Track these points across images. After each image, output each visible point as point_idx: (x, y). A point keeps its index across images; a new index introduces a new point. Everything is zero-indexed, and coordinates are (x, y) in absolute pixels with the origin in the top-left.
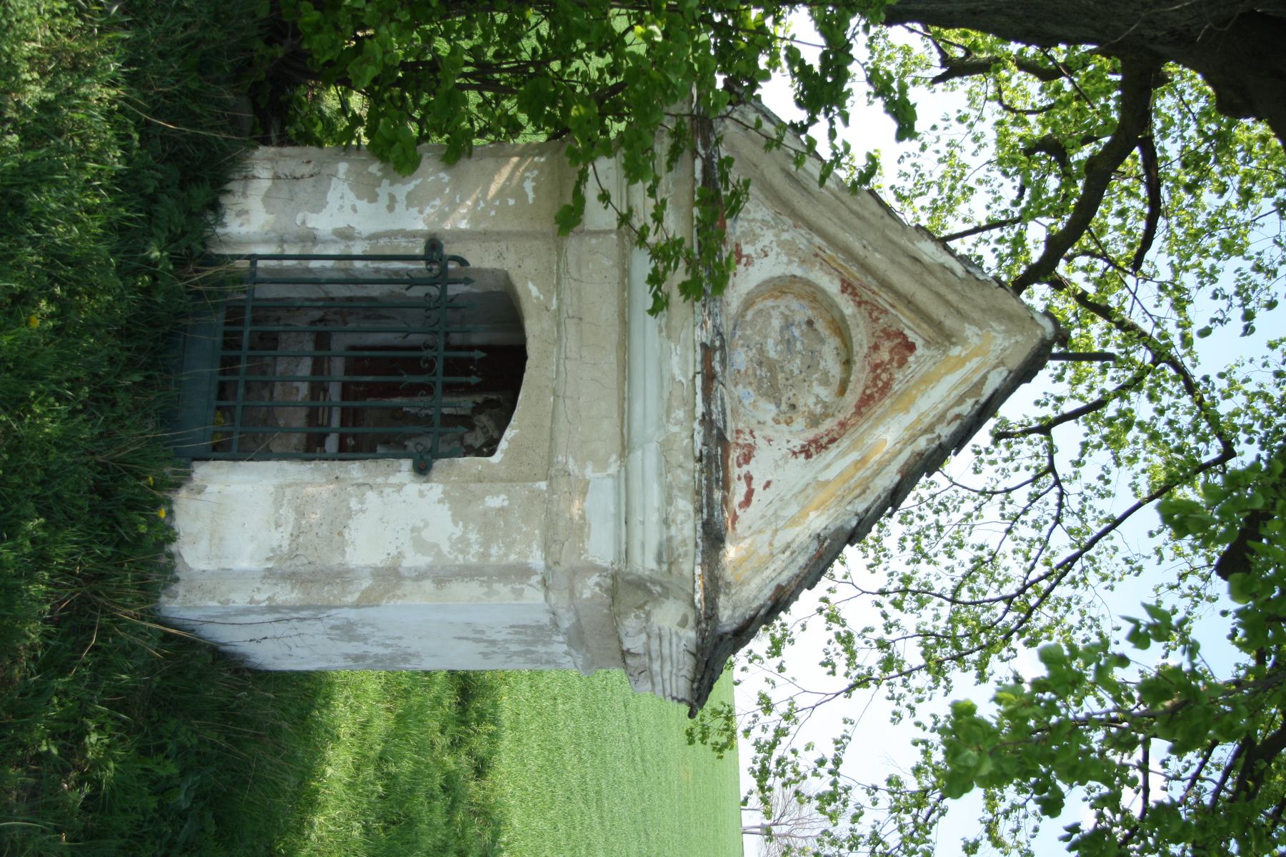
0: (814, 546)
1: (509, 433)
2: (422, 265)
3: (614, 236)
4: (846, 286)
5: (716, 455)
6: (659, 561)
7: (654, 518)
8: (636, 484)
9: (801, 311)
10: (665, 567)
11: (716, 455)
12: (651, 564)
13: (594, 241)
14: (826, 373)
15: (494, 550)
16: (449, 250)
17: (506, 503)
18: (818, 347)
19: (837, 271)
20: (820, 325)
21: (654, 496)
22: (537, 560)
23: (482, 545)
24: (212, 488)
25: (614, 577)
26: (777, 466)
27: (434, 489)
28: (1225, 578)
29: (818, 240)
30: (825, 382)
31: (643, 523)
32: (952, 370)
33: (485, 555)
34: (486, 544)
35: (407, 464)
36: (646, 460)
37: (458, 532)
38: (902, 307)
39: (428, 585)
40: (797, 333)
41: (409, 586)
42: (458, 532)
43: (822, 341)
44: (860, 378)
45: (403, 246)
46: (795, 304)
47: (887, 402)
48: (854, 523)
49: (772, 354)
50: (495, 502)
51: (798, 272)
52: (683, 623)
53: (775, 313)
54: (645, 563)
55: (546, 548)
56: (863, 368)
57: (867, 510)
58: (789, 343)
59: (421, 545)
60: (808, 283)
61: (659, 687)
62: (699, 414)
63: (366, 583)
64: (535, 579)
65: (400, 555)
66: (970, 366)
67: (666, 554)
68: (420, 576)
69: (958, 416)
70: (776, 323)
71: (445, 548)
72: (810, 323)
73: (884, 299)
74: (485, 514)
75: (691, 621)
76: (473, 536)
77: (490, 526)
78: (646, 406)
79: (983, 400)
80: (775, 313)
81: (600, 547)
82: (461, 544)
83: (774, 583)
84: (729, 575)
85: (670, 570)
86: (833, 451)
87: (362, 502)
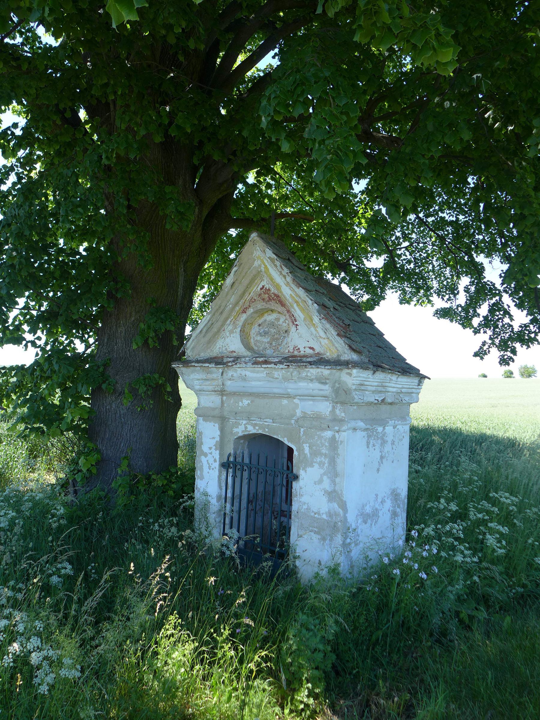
0: (323, 321)
1: (286, 442)
2: (231, 470)
3: (225, 398)
4: (244, 312)
5: (294, 360)
6: (325, 383)
7: (311, 385)
8: (300, 392)
9: (254, 330)
10: (327, 381)
11: (294, 360)
12: (327, 387)
13: (225, 405)
14: (276, 319)
15: (324, 451)
16: (225, 460)
17: (308, 445)
18: (267, 322)
19: (238, 315)
20: (260, 321)
21: (303, 384)
22: (328, 434)
23: (321, 456)
24: (333, 564)
25: (337, 403)
26: (301, 337)
27: (302, 474)
28: (289, 142)
29: (228, 322)
30: (278, 319)
31: (313, 390)
32: (268, 270)
33: (325, 455)
34: (321, 454)
35: (294, 483)
36: (291, 387)
37: (316, 466)
38: (250, 290)
39: (337, 480)
40: (262, 330)
41: (337, 488)
42: (316, 466)
43: (265, 320)
44: (274, 305)
45: (224, 477)
46: (253, 331)
47: (280, 295)
48: (316, 305)
49: (269, 340)
50: (307, 450)
51: (239, 329)
52: (350, 374)
53: (256, 339)
54: (327, 389)
55: (323, 430)
56: (270, 304)
57: (311, 300)
58: (266, 333)
59: (320, 481)
60: (244, 326)
61: (414, 390)
62: (275, 366)
63: (336, 505)
64: (337, 435)
65: (324, 489)
66: (267, 264)
67: (322, 381)
68: (334, 482)
69: (281, 266)
70: (259, 338)
71: (322, 471)
72: (259, 325)
73: (247, 297)
74: (311, 454)
75: (349, 371)
76: (318, 460)
77: (315, 453)
78: (276, 388)
79: (276, 257)
80: (256, 339)
81: (324, 408)
82: (321, 464)
83: (336, 337)
84: (335, 356)
85: (328, 379)
86: (295, 315)
87: (305, 503)
